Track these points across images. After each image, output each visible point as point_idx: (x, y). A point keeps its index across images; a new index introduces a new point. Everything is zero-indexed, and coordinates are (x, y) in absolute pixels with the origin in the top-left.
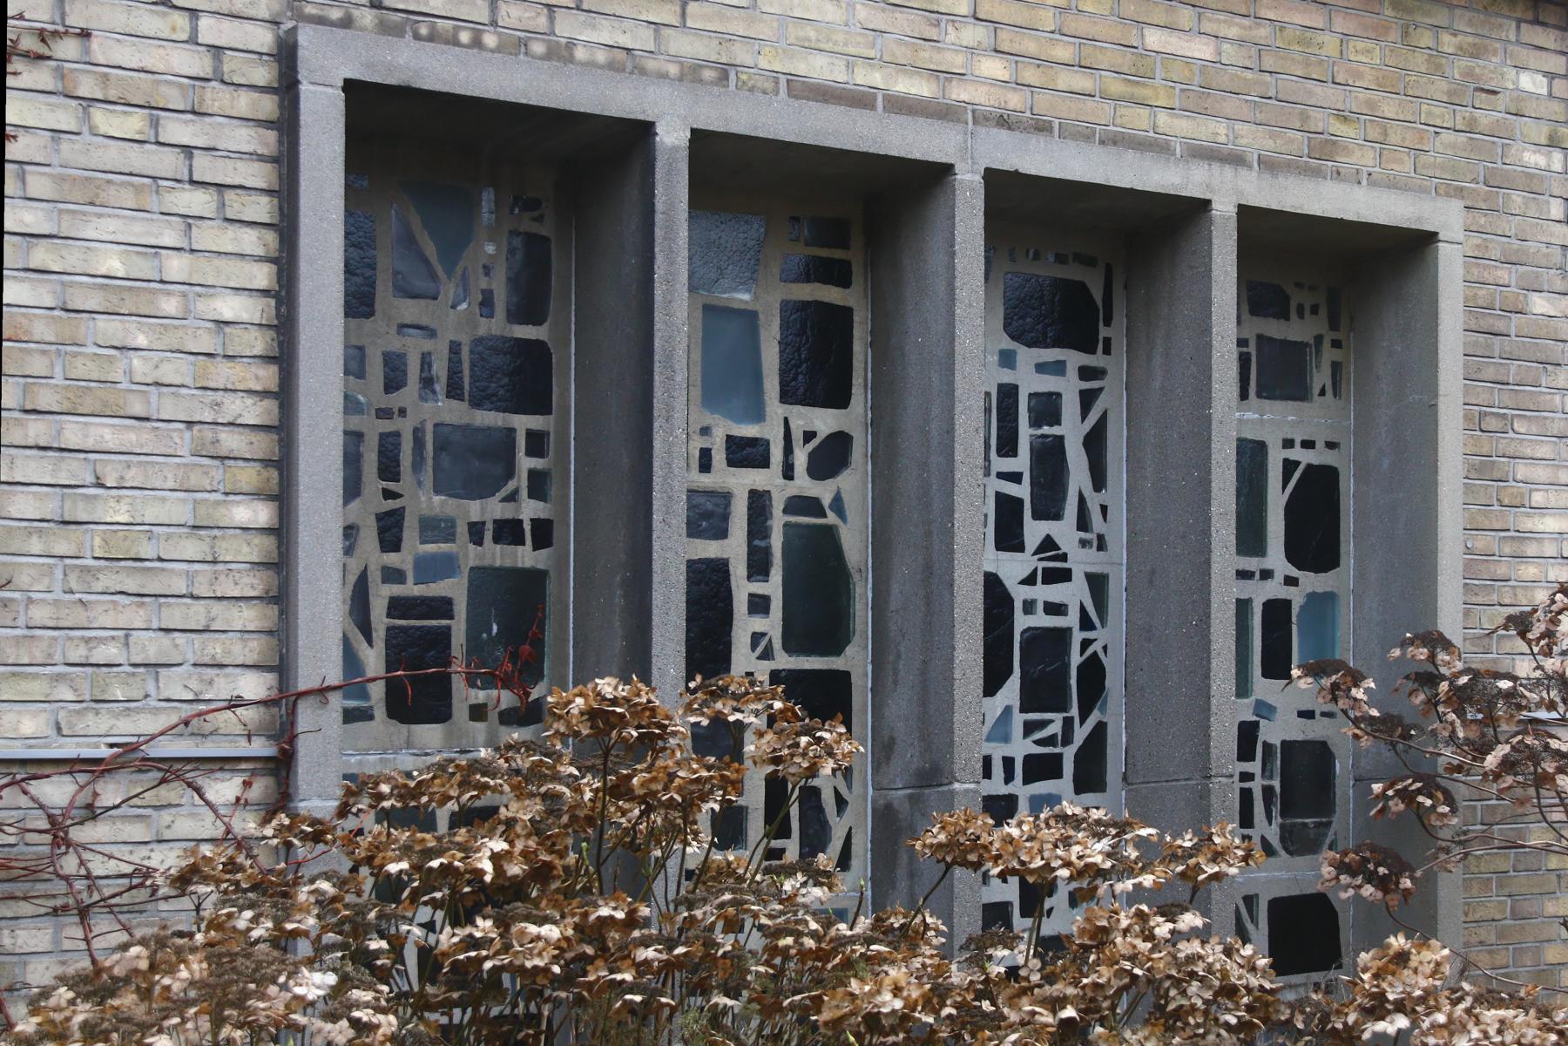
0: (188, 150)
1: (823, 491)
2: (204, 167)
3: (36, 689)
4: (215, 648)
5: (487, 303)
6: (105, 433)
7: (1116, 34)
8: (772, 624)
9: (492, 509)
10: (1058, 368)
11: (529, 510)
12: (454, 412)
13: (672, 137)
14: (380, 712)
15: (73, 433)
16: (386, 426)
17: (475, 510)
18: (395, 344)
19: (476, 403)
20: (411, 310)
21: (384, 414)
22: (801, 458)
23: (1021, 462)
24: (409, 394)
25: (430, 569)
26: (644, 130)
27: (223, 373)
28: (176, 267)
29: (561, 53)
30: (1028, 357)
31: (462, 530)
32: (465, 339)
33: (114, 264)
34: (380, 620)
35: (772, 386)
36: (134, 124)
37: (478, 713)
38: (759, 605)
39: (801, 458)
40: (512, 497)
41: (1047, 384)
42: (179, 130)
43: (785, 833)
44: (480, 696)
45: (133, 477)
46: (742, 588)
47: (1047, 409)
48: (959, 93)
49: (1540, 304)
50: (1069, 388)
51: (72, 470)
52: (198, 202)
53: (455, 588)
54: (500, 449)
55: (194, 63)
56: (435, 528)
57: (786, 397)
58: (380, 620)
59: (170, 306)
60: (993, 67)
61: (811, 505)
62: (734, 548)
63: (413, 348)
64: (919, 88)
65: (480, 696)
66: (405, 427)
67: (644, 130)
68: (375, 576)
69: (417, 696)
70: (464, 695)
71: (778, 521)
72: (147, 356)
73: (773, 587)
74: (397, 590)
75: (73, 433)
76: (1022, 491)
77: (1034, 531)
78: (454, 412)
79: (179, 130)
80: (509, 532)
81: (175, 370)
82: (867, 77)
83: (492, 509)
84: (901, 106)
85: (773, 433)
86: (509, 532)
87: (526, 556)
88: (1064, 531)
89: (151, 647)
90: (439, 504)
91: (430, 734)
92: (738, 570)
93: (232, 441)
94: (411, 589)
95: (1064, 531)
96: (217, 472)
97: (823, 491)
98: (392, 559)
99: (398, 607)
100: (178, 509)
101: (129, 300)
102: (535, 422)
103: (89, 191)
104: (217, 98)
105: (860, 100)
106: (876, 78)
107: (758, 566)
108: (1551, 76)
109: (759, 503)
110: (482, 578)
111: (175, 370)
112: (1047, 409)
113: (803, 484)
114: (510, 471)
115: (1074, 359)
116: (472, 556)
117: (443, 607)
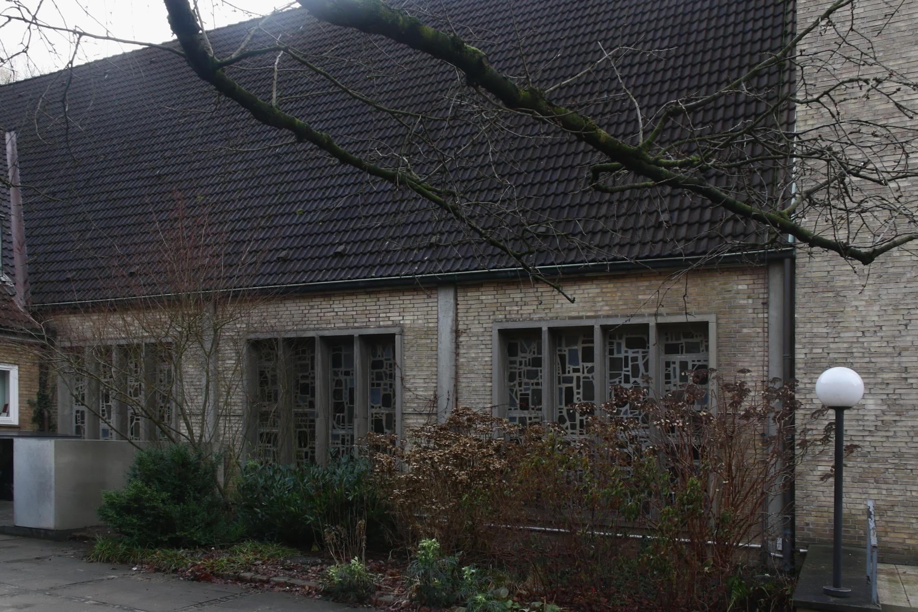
1: (590, 376)
2: (484, 342)
6: (472, 375)
8: (581, 396)
10: (638, 352)
12: (529, 368)
13: (545, 329)
15: (469, 376)
17: (532, 381)
20: (523, 355)
22: (586, 371)
23: (630, 368)
24: (523, 366)
25: (526, 389)
26: (540, 329)
28: (481, 355)
29: (531, 320)
30: (630, 351)
33: (473, 355)
34: (519, 396)
35: (580, 360)
36: (475, 338)
38: (578, 393)
39: (586, 371)
41: (635, 355)
42: (481, 338)
43: (272, 397)
46: (575, 391)
47: (635, 359)
48: (600, 313)
49: (745, 331)
50: (640, 356)
51: (469, 380)
52: (483, 347)
53: (530, 392)
55: (482, 330)
56: (526, 384)
57: (583, 361)
58: (519, 396)
60: (607, 308)
61: (588, 378)
62: (574, 385)
63: (523, 360)
64: (592, 314)
67: (540, 329)
71: (582, 380)
72: (477, 366)
73: (581, 390)
75: (469, 376)
76: (630, 373)
77: (632, 380)
78: (529, 368)
79: (481, 338)
81: (481, 367)
82: (581, 314)
84: (588, 317)
85: (580, 367)
88: (639, 380)
89: (478, 401)
90: (527, 380)
91: (526, 412)
92: (575, 388)
95: (639, 380)
97: (590, 376)
100: (481, 384)
101: (475, 359)
103: (470, 347)
104: (485, 333)
105: (581, 318)
106: (584, 314)
107: (578, 387)
108: (748, 285)
109: (578, 378)
111: (481, 367)
112: (635, 359)
113: (586, 374)
115: (641, 350)
116: (532, 387)
117: (528, 395)
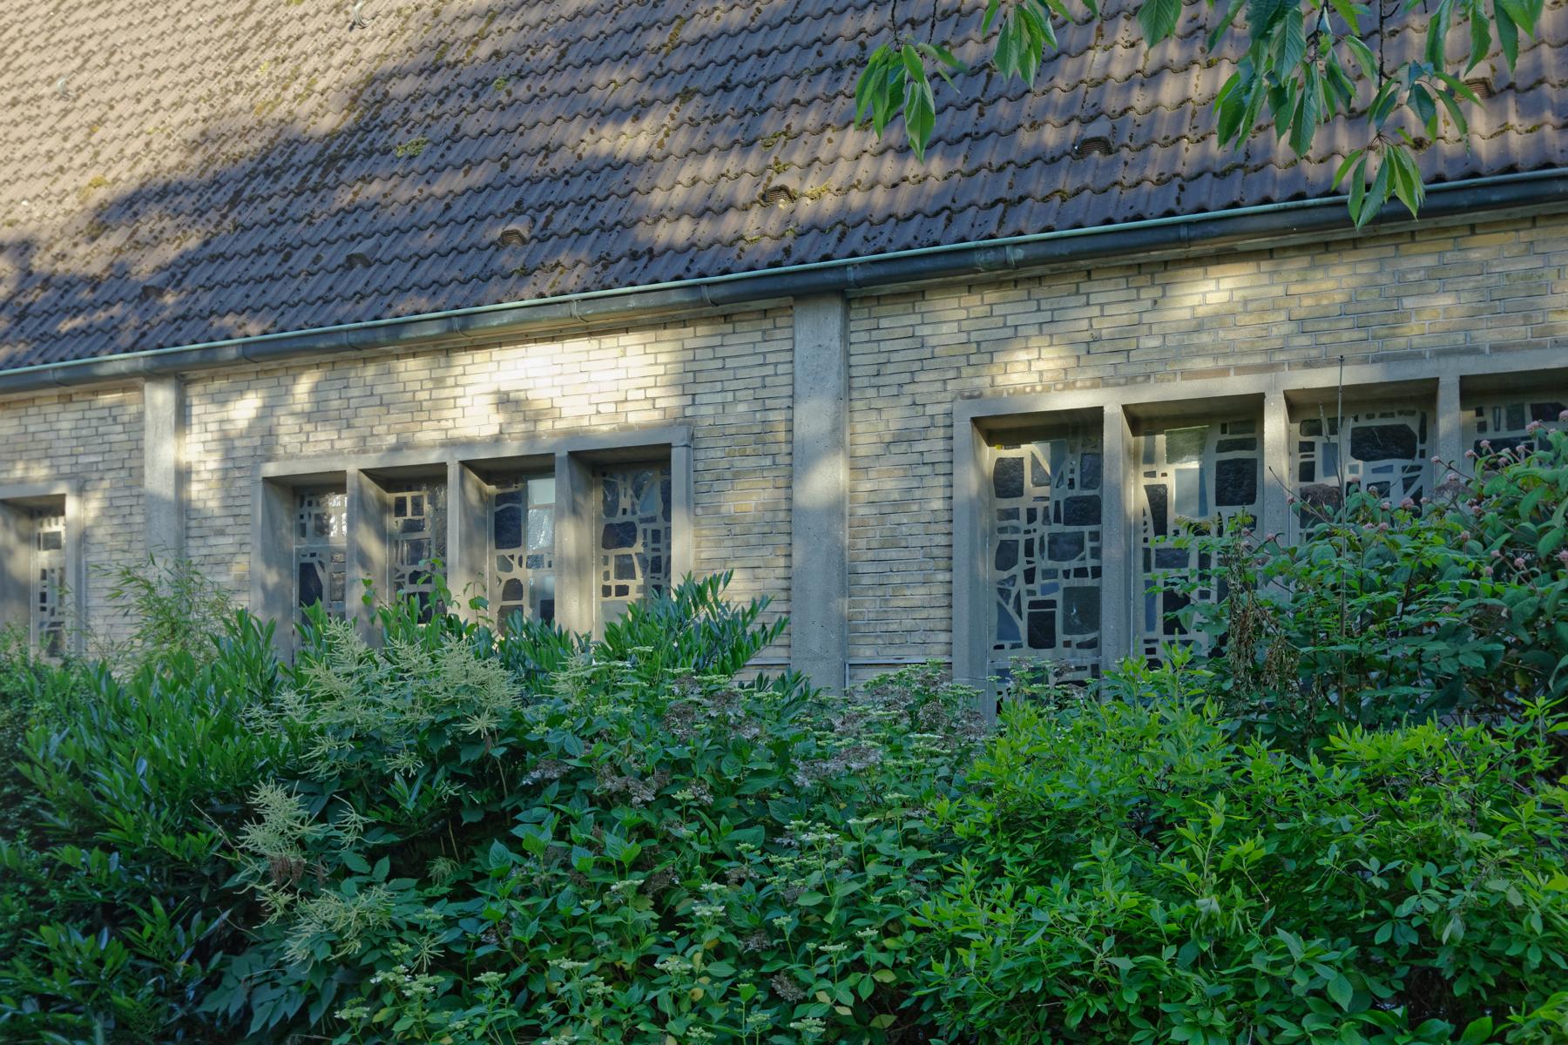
0: (922, 453)
3: (870, 640)
4: (930, 625)
5: (1071, 484)
6: (893, 554)
7: (1384, 306)
9: (1074, 564)
10: (1389, 469)
11: (1090, 563)
14: (1025, 644)
16: (1028, 537)
17: (1066, 565)
18: (1032, 505)
19: (1067, 523)
21: (1028, 532)
24: (1037, 524)
25: (1045, 590)
27: (933, 528)
31: (1060, 573)
32: (1062, 500)
37: (1067, 644)
40: (1083, 559)
44: (1068, 638)
45: (902, 567)
52: (926, 470)
53: (1058, 596)
54: (1079, 541)
56: (1048, 574)
59: (915, 507)
65: (1068, 638)
66: (1036, 537)
68: (1023, 594)
69: (1041, 636)
70: (1061, 638)
74: (1032, 598)
75: (883, 555)
78: (1058, 528)
80: (1081, 573)
81: (917, 529)
83: (1074, 564)
86: (1081, 573)
87: (1088, 582)
93: (937, 552)
94: (1039, 597)
96: (932, 563)
98: (1030, 587)
99: (1032, 605)
102: (1093, 528)
110: (1069, 592)
111: (917, 529)
114: (1082, 548)
115: (1398, 463)
116: (1064, 583)
117: (1052, 604)
